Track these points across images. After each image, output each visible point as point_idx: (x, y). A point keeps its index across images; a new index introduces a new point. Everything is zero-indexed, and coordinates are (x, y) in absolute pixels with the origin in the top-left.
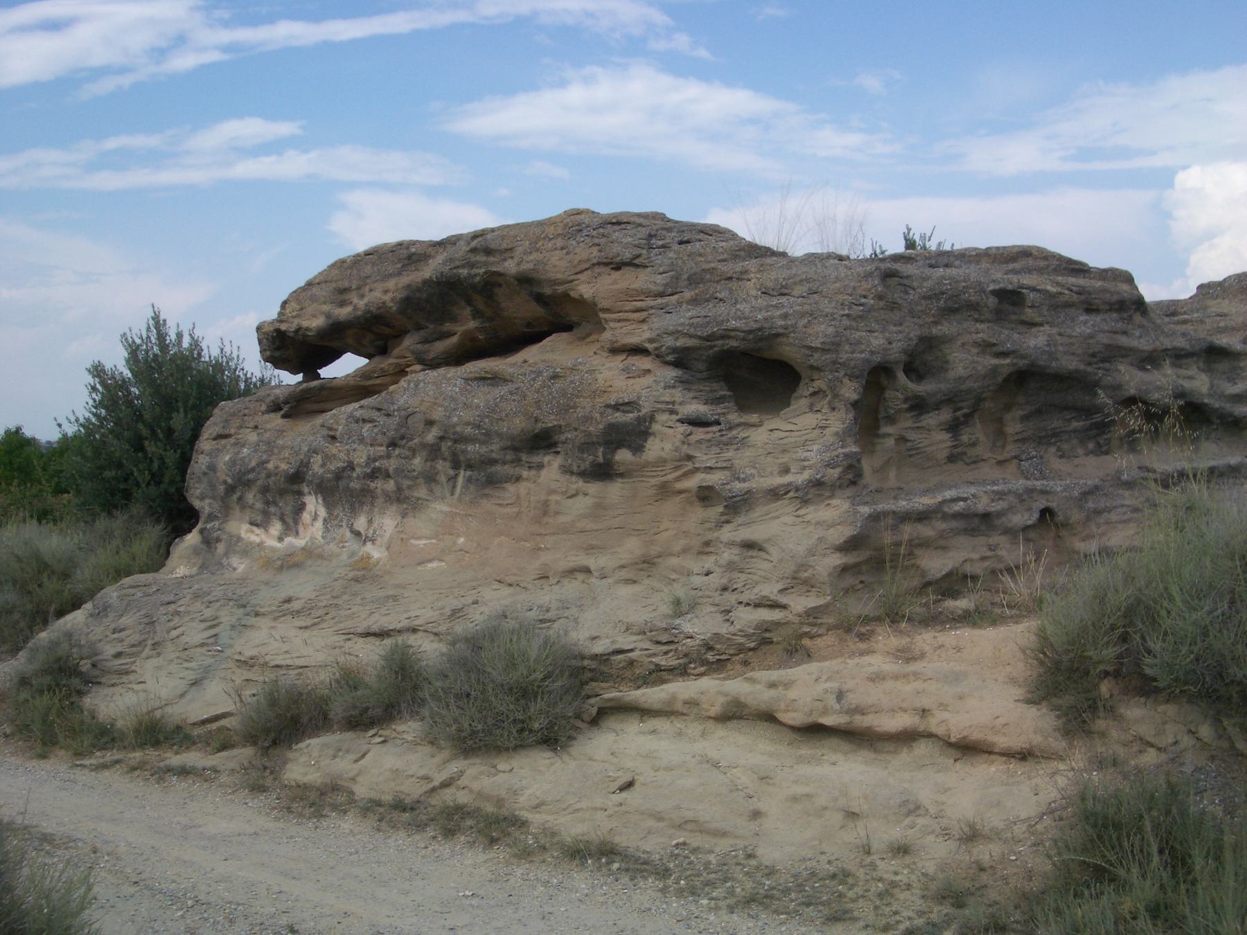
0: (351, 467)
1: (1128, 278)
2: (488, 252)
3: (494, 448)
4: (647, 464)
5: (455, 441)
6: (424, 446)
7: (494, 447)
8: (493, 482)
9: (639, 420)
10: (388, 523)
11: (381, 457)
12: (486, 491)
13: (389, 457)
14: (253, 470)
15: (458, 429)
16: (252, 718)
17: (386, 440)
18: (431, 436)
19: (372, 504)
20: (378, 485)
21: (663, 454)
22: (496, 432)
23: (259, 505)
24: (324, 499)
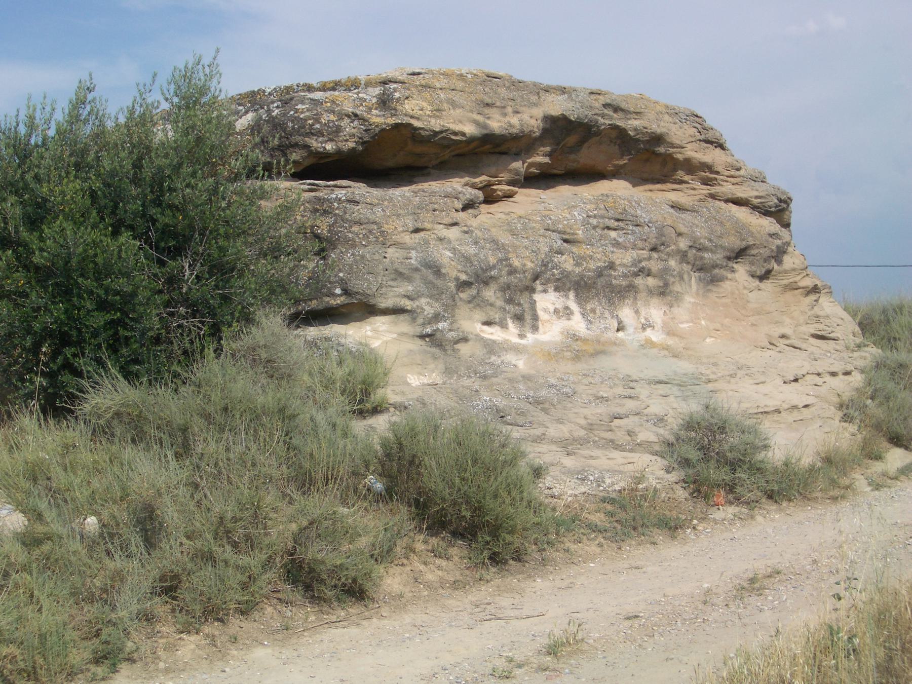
0: (612, 266)
1: (634, 186)
2: (617, 109)
3: (718, 257)
4: (786, 272)
5: (699, 250)
6: (679, 251)
7: (718, 256)
8: (715, 280)
9: (784, 244)
10: (655, 312)
11: (644, 259)
12: (710, 287)
13: (650, 258)
14: (494, 267)
15: (702, 241)
16: (766, 447)
17: (648, 246)
18: (683, 244)
19: (635, 299)
20: (639, 281)
21: (795, 266)
22: (721, 246)
23: (500, 303)
24: (577, 296)
